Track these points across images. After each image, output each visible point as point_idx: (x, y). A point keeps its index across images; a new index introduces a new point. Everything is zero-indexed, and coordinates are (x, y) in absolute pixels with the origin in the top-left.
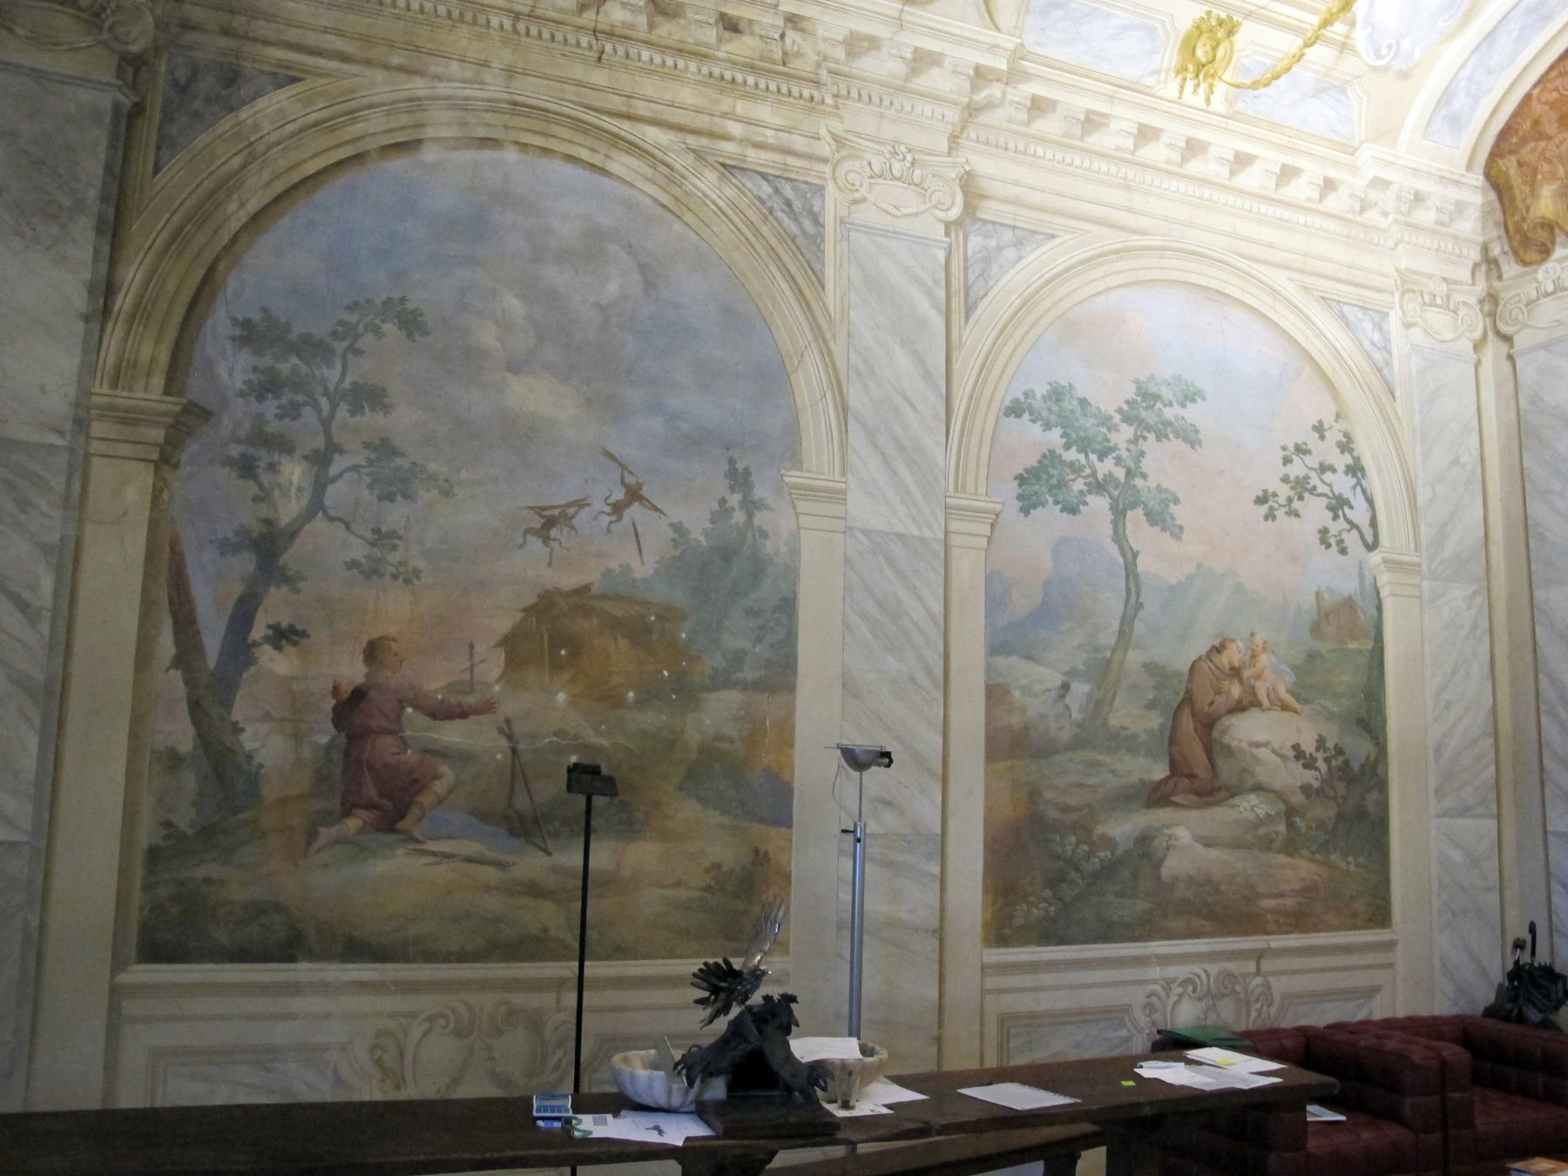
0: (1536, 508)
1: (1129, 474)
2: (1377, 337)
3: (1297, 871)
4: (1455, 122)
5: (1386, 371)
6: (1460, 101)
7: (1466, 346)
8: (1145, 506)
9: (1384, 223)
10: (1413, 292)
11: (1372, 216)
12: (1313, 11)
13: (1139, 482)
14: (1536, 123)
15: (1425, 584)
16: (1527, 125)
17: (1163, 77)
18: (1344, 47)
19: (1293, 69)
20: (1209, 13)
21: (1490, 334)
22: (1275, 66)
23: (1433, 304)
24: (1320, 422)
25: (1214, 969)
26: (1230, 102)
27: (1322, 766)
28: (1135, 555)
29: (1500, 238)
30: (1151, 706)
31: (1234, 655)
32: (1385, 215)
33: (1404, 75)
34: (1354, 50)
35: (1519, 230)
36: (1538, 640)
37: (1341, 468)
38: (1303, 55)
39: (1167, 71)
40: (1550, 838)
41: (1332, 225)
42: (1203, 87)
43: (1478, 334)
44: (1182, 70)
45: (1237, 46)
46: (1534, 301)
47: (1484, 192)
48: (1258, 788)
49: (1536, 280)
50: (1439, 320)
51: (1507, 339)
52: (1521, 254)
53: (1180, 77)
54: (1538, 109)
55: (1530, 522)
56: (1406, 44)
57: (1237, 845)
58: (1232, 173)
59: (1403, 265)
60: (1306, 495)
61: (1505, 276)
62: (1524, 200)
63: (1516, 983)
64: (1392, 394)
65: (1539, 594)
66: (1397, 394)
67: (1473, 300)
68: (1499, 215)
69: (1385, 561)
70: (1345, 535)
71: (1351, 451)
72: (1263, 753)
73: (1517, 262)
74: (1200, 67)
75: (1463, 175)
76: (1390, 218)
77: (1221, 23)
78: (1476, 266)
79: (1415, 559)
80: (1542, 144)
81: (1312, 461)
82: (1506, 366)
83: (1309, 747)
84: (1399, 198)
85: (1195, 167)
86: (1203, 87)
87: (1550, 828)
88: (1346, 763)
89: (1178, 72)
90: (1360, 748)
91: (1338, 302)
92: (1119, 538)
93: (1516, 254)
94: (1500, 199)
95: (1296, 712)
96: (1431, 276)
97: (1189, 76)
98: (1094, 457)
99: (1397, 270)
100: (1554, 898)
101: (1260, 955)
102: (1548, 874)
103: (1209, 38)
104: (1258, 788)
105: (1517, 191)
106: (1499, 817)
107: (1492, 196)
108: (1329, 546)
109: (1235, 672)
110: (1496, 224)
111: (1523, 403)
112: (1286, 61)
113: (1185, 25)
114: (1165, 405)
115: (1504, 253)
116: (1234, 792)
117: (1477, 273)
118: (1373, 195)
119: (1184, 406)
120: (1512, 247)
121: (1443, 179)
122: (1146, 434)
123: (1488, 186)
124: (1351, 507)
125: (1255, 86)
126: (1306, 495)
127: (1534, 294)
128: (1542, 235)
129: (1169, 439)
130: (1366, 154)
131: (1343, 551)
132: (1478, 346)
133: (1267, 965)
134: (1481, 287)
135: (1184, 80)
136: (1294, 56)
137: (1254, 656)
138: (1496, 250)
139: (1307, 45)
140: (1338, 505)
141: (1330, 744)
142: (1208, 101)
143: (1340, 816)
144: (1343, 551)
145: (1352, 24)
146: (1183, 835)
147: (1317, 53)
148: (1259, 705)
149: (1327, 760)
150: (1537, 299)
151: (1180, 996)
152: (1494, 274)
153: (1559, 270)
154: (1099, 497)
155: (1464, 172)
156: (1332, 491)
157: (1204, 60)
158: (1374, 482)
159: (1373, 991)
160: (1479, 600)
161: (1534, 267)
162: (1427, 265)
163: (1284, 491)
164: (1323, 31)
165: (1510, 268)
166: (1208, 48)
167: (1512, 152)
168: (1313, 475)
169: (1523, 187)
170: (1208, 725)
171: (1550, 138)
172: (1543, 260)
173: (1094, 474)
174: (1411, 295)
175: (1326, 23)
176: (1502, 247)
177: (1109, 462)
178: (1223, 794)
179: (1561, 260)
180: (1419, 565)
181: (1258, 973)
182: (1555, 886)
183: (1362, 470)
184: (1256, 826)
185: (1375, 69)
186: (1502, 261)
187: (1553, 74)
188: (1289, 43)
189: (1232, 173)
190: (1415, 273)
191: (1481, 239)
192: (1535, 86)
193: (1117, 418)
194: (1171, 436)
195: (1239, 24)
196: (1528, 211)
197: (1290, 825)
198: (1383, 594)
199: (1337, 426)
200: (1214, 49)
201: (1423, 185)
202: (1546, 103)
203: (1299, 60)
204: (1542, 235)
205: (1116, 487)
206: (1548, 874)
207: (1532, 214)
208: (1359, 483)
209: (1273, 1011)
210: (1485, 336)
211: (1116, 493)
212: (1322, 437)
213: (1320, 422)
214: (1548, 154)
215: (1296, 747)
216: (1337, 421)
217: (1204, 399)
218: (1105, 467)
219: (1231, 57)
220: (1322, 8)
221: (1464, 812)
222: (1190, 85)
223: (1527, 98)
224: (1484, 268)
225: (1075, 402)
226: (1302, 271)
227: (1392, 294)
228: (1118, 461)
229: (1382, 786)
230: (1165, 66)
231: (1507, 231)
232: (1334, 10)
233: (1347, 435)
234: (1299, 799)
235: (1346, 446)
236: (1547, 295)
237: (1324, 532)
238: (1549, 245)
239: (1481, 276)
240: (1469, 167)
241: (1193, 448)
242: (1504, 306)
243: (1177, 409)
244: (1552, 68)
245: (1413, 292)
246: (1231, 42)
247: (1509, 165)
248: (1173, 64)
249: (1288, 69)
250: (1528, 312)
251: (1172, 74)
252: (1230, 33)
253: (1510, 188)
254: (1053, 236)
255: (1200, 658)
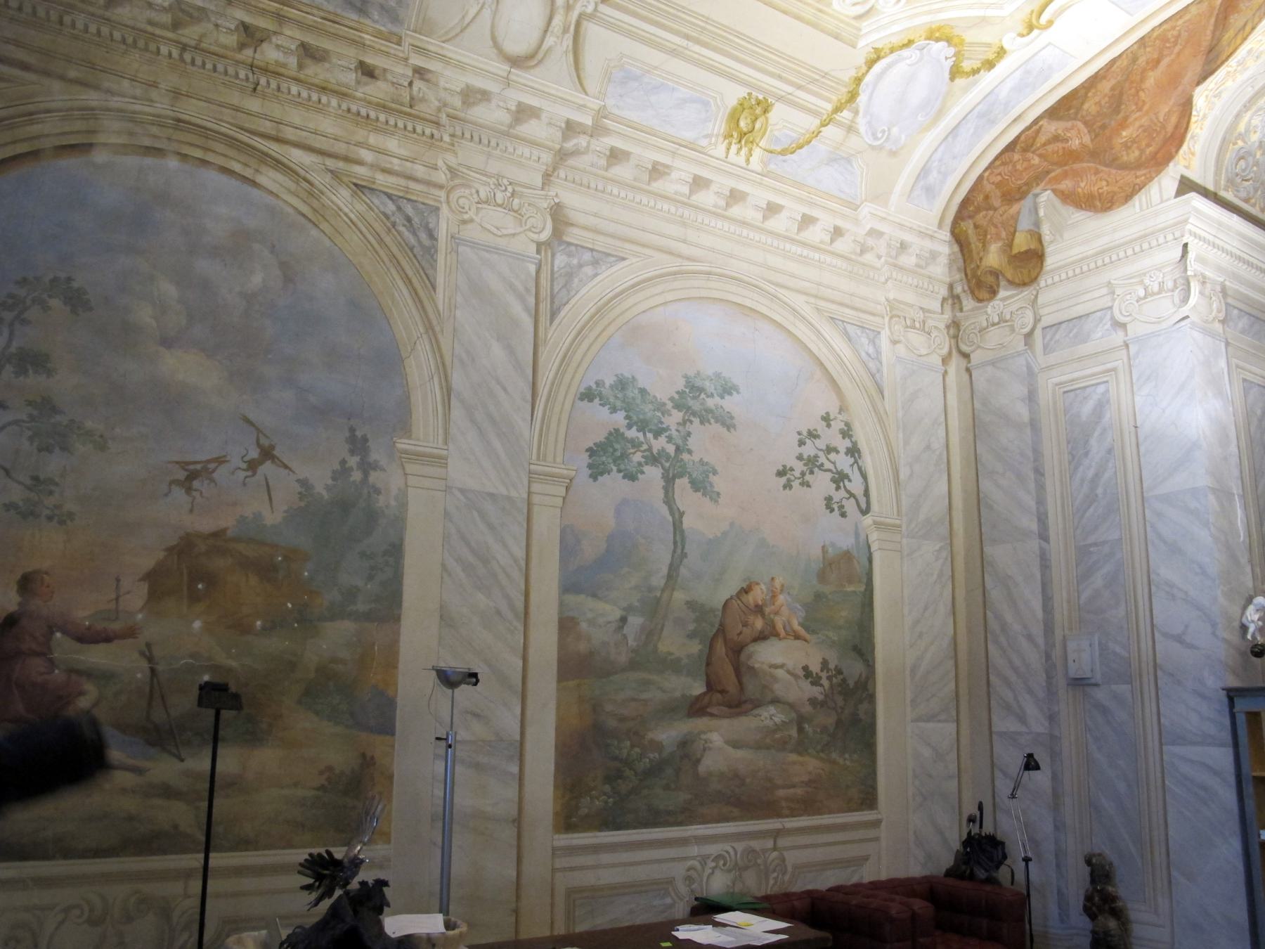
0: (986, 485)
1: (678, 449)
2: (871, 350)
3: (808, 765)
4: (930, 191)
5: (878, 376)
6: (933, 177)
7: (936, 360)
8: (690, 476)
9: (878, 264)
10: (899, 317)
11: (869, 258)
12: (828, 100)
13: (685, 456)
14: (987, 197)
15: (904, 541)
16: (980, 198)
17: (713, 140)
18: (851, 129)
19: (813, 142)
20: (750, 94)
21: (954, 352)
22: (800, 138)
23: (914, 328)
24: (827, 413)
25: (740, 846)
26: (765, 164)
27: (825, 683)
28: (682, 514)
29: (961, 280)
30: (692, 636)
31: (758, 595)
32: (879, 257)
33: (893, 153)
34: (857, 132)
35: (974, 271)
36: (986, 585)
37: (842, 450)
38: (820, 132)
39: (717, 136)
40: (994, 737)
41: (839, 262)
42: (744, 151)
43: (945, 351)
44: (728, 136)
45: (771, 122)
46: (985, 329)
47: (951, 246)
48: (775, 701)
49: (986, 312)
50: (916, 338)
51: (966, 356)
52: (976, 292)
53: (727, 141)
54: (988, 187)
55: (981, 495)
56: (895, 130)
57: (758, 746)
58: (765, 218)
59: (891, 296)
60: (816, 470)
61: (965, 309)
62: (978, 253)
63: (968, 850)
64: (882, 393)
65: (987, 549)
66: (886, 394)
67: (942, 326)
68: (961, 261)
69: (875, 523)
70: (844, 502)
71: (850, 437)
72: (780, 673)
73: (973, 299)
74: (742, 135)
75: (935, 232)
76: (883, 259)
77: (759, 103)
78: (944, 300)
79: (898, 522)
80: (991, 213)
81: (821, 444)
82: (966, 377)
83: (815, 668)
84: (889, 245)
85: (736, 211)
86: (744, 151)
87: (994, 729)
88: (844, 680)
89: (725, 138)
90: (855, 669)
91: (843, 321)
92: (669, 501)
93: (972, 293)
94: (962, 251)
95: (806, 640)
96: (912, 306)
97: (734, 141)
98: (650, 436)
99: (887, 300)
100: (997, 783)
101: (777, 834)
102: (993, 765)
103: (751, 114)
104: (775, 701)
105: (973, 246)
106: (958, 721)
107: (956, 248)
108: (832, 510)
109: (759, 610)
110: (959, 269)
111: (977, 405)
112: (808, 136)
113: (732, 102)
114: (708, 397)
115: (964, 291)
116: (757, 704)
117: (945, 305)
118: (870, 242)
119: (722, 398)
120: (970, 288)
121: (922, 234)
122: (692, 418)
123: (953, 240)
124: (850, 481)
125: (783, 152)
126: (816, 470)
127: (985, 324)
128: (990, 279)
129: (710, 424)
130: (866, 210)
131: (843, 515)
132: (945, 361)
133: (782, 842)
134: (947, 316)
135: (730, 144)
136: (813, 133)
137: (774, 597)
138: (958, 289)
139: (823, 125)
140: (840, 478)
141: (832, 666)
142: (748, 161)
143: (839, 723)
144: (843, 515)
145: (856, 113)
146: (716, 739)
147: (829, 131)
148: (777, 635)
149: (829, 678)
150: (987, 327)
151: (714, 869)
152: (957, 306)
153: (1002, 306)
154: (653, 467)
155: (936, 230)
156: (836, 468)
157: (745, 130)
158: (868, 462)
159: (864, 859)
160: (945, 554)
161: (986, 303)
162: (910, 297)
163: (799, 467)
164: (835, 115)
165: (968, 303)
166: (749, 121)
167: (970, 217)
168: (821, 454)
169: (978, 244)
170: (737, 650)
171: (995, 209)
172: (991, 299)
173: (650, 449)
174: (897, 319)
175: (837, 110)
176: (963, 288)
177: (662, 440)
178: (749, 706)
179: (1003, 300)
180: (900, 526)
181: (775, 849)
182: (998, 774)
183: (859, 451)
184: (775, 731)
185: (873, 147)
186: (963, 296)
187: (998, 163)
188: (812, 123)
189: (765, 218)
190: (900, 302)
191: (948, 280)
192: (986, 169)
193: (670, 405)
194: (712, 421)
195: (772, 105)
196: (981, 259)
197: (801, 730)
198: (874, 547)
199: (840, 417)
200: (754, 122)
201: (908, 237)
202: (993, 183)
203: (817, 136)
204: (990, 279)
205: (667, 461)
206: (993, 765)
207: (984, 263)
208: (856, 462)
209: (787, 878)
210: (950, 353)
211: (667, 465)
212: (829, 426)
213: (827, 413)
214: (995, 221)
215: (805, 668)
216: (840, 413)
217: (738, 393)
218: (659, 444)
219: (766, 130)
220: (834, 98)
221: (931, 718)
222: (734, 148)
223: (980, 178)
224: (950, 302)
225: (636, 391)
226: (816, 297)
227: (883, 317)
228: (670, 439)
229: (872, 698)
230: (715, 132)
231: (966, 275)
232: (843, 101)
233: (847, 424)
234: (807, 709)
235: (846, 433)
236: (994, 325)
237: (829, 500)
238: (995, 287)
239: (948, 307)
240: (940, 226)
241: (728, 430)
242: (964, 331)
243: (717, 399)
244: (996, 158)
245: (899, 317)
246: (767, 119)
247: (968, 226)
248: (722, 131)
249: (808, 142)
250: (981, 336)
251: (721, 139)
252: (766, 111)
253: (970, 244)
254: (624, 259)
255: (732, 598)
